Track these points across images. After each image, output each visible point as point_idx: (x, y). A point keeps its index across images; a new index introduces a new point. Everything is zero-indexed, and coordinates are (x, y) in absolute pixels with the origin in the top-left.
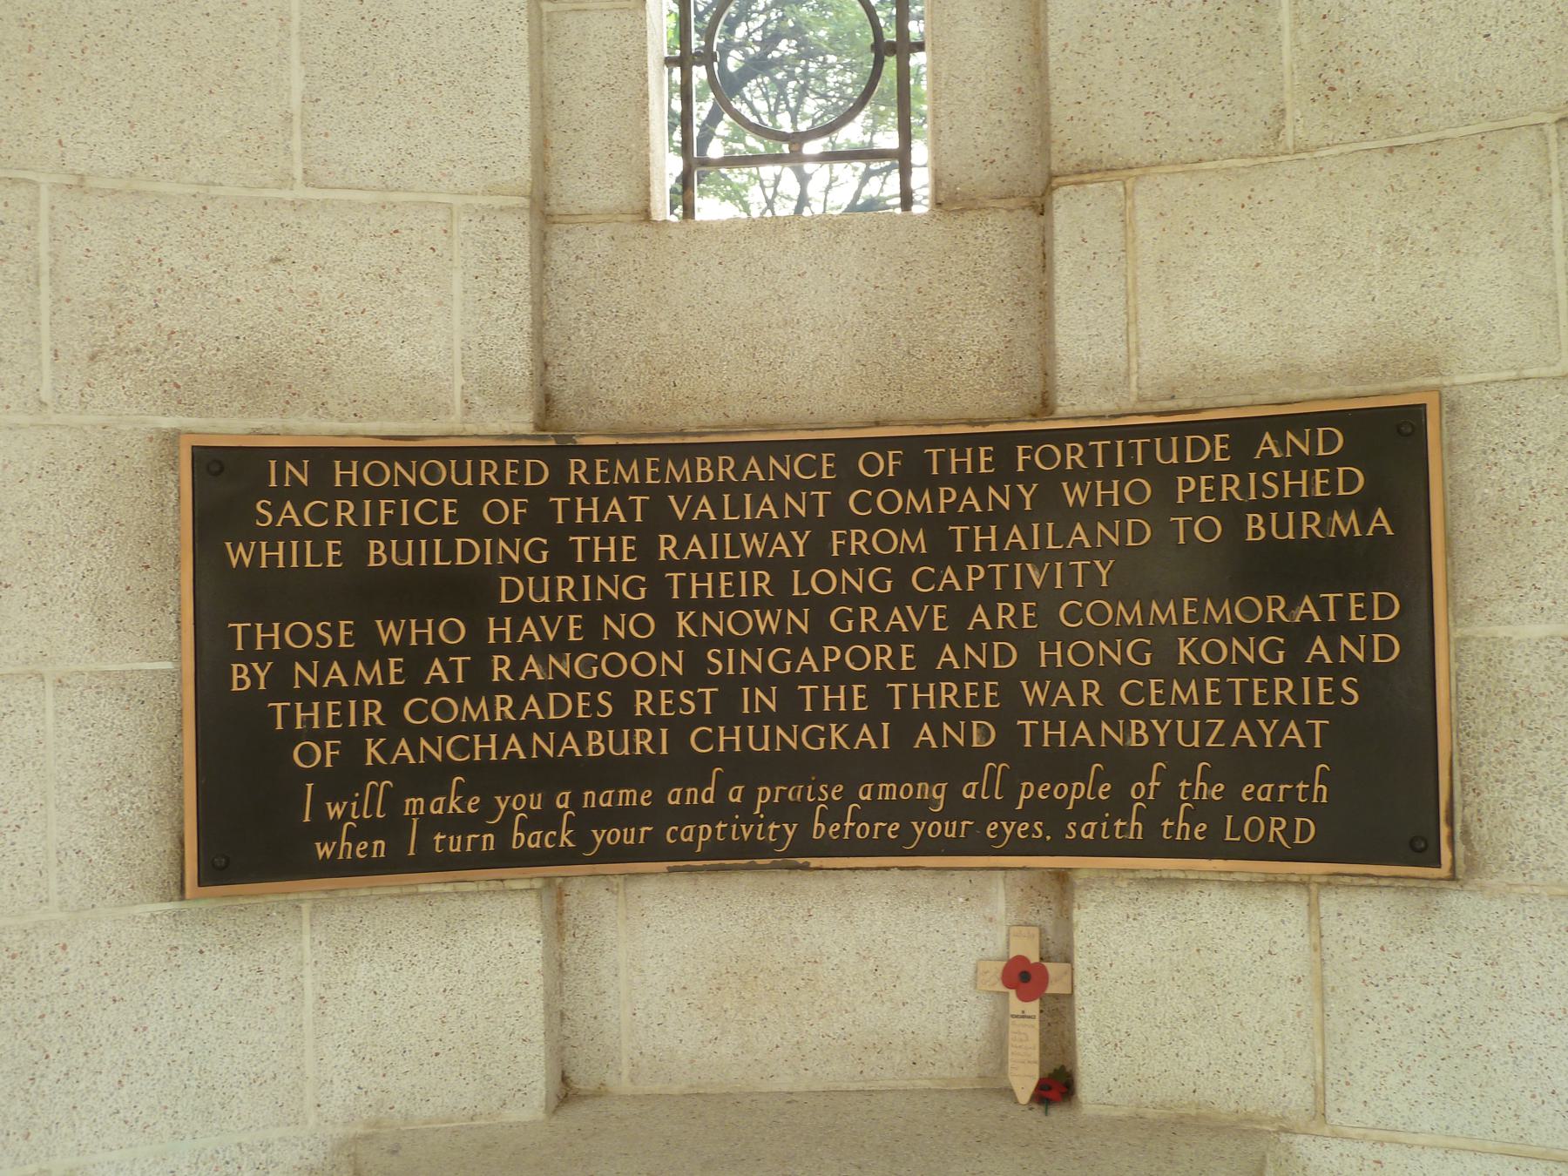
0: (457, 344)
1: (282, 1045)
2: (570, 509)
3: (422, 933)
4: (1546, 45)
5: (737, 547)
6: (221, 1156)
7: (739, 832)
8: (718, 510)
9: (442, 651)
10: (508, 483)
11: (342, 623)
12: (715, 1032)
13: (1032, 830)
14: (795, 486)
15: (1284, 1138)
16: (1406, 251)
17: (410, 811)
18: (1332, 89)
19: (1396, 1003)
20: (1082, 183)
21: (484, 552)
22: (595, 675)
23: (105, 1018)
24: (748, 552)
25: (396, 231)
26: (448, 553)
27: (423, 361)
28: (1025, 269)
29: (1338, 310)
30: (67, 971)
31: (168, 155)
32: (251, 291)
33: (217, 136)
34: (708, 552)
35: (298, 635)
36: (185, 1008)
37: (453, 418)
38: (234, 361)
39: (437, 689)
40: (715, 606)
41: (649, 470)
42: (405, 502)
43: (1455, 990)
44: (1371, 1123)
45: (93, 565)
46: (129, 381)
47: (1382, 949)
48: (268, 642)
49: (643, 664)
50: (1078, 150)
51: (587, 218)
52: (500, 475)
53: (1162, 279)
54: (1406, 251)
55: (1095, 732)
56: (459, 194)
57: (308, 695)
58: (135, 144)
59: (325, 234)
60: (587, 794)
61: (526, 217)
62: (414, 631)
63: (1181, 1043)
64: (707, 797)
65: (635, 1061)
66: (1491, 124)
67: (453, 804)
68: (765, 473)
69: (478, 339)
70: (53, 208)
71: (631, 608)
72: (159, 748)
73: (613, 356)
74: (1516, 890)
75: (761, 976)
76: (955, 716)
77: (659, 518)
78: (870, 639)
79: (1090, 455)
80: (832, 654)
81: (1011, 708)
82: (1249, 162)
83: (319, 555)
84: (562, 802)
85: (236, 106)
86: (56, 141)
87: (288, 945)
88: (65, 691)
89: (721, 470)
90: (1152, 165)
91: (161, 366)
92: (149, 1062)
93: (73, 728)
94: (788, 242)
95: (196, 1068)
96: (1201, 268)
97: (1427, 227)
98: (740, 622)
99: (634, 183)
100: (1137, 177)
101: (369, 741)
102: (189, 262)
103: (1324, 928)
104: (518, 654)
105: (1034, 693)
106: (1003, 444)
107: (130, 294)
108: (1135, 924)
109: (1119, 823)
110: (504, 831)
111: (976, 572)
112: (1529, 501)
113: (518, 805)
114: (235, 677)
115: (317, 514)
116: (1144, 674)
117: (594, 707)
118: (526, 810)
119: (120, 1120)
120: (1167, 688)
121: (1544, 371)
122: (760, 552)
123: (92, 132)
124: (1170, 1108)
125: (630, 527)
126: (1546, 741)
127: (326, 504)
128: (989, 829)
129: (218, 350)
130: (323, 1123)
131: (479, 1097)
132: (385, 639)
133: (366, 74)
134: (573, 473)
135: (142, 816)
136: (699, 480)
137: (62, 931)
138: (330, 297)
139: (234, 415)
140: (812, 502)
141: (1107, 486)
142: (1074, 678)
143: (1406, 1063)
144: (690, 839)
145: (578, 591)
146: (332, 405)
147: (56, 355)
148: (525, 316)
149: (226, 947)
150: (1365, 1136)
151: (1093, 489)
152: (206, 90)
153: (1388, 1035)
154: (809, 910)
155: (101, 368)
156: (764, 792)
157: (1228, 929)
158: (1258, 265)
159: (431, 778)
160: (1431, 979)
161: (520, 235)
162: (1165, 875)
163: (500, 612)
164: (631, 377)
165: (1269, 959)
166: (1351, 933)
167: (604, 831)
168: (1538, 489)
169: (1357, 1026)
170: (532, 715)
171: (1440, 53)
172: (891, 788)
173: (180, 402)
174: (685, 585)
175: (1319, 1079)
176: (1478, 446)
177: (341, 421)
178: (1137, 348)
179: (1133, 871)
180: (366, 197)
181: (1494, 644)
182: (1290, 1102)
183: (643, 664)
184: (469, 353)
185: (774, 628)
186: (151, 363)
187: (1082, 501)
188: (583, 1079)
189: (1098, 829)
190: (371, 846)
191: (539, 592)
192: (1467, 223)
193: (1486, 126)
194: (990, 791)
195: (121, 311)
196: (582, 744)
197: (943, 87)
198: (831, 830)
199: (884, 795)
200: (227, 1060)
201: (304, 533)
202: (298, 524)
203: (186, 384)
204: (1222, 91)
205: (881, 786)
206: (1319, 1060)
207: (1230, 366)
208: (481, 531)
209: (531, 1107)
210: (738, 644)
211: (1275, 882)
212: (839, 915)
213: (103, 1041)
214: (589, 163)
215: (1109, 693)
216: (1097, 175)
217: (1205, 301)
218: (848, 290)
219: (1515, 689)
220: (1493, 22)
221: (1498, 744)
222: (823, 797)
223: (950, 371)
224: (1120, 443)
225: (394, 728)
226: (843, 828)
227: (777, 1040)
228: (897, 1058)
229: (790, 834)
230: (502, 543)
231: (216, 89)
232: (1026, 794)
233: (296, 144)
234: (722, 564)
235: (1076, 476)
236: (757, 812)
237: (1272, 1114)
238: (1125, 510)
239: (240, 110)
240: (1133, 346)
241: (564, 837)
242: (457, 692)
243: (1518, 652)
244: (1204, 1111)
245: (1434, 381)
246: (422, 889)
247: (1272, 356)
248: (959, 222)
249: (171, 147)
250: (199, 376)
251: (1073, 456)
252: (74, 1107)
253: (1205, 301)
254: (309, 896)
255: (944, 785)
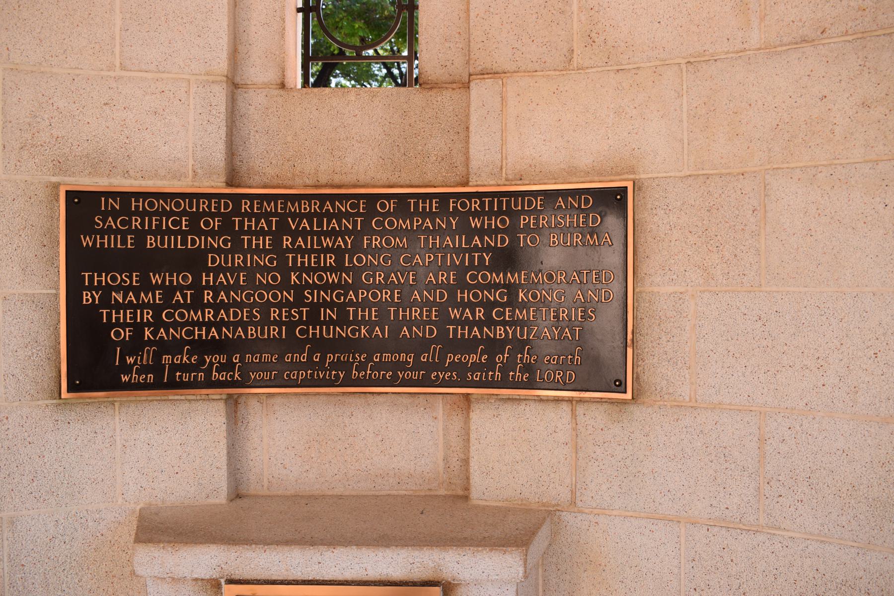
0: (190, 145)
1: (106, 466)
2: (241, 223)
3: (171, 418)
4: (683, 28)
5: (320, 243)
6: (78, 515)
7: (318, 375)
8: (311, 226)
9: (181, 288)
10: (213, 210)
11: (134, 274)
12: (307, 467)
13: (452, 376)
14: (347, 215)
15: (558, 513)
16: (623, 117)
17: (165, 361)
18: (594, 42)
19: (606, 453)
20: (484, 78)
21: (200, 242)
22: (252, 301)
23: (25, 451)
24: (325, 245)
25: (163, 92)
26: (184, 242)
27: (175, 152)
28: (459, 117)
29: (594, 143)
30: (8, 429)
31: (57, 55)
32: (94, 119)
33: (80, 46)
34: (306, 244)
35: (114, 279)
36: (62, 448)
37: (188, 180)
38: (86, 151)
39: (178, 305)
40: (309, 270)
41: (279, 206)
42: (164, 218)
43: (631, 447)
44: (594, 506)
45: (20, 245)
46: (37, 160)
47: (602, 430)
48: (100, 282)
49: (275, 296)
50: (482, 63)
51: (255, 86)
52: (209, 207)
53: (518, 124)
54: (623, 117)
55: (481, 332)
56: (193, 74)
57: (118, 306)
58: (42, 50)
59: (129, 92)
60: (247, 356)
61: (225, 85)
62: (168, 278)
63: (516, 472)
64: (304, 359)
65: (270, 480)
66: (659, 62)
67: (185, 359)
68: (334, 209)
69: (201, 143)
70: (4, 79)
71: (269, 270)
72: (50, 329)
73: (265, 152)
74: (657, 403)
75: (329, 442)
76: (420, 324)
77: (282, 227)
78: (380, 287)
79: (482, 204)
80: (363, 293)
81: (444, 319)
82: (557, 73)
83: (124, 242)
84: (236, 359)
85: (89, 32)
86: (6, 48)
87: (109, 421)
88: (6, 302)
89: (313, 207)
90: (515, 72)
91: (52, 153)
92: (45, 471)
93: (10, 319)
94: (349, 100)
95: (67, 475)
96: (535, 120)
97: (632, 107)
98: (320, 278)
99: (277, 70)
100: (508, 77)
101: (146, 329)
102: (66, 104)
103: (578, 420)
104: (216, 291)
105: (455, 313)
106: (444, 198)
107: (38, 120)
108: (497, 419)
109: (490, 373)
110: (208, 372)
111: (429, 257)
112: (669, 232)
113: (215, 360)
114: (85, 297)
115: (123, 223)
116: (503, 305)
117: (251, 315)
118: (219, 362)
119: (33, 496)
120: (513, 311)
121: (678, 174)
122: (330, 245)
123: (23, 44)
124: (510, 501)
125: (270, 232)
126: (672, 338)
127: (127, 219)
128: (433, 375)
129: (79, 146)
130: (125, 502)
131: (197, 493)
132: (154, 282)
133: (150, 18)
134: (243, 206)
135: (42, 360)
136: (303, 211)
137: (6, 411)
138: (131, 122)
139: (86, 176)
140: (355, 223)
141: (490, 219)
142: (472, 306)
143: (610, 479)
144: (295, 377)
145: (245, 261)
146: (131, 173)
147: (4, 147)
148: (223, 132)
149: (80, 421)
150: (592, 512)
151: (484, 220)
152: (75, 25)
153: (603, 467)
154: (352, 413)
155: (25, 154)
156: (330, 357)
157: (537, 421)
158: (560, 120)
159: (175, 347)
160: (622, 443)
161: (222, 94)
162: (511, 397)
163: (208, 271)
164: (274, 162)
165: (554, 434)
166: (589, 423)
167: (255, 373)
168: (673, 226)
169: (590, 464)
170: (222, 319)
171: (640, 29)
172: (388, 356)
173: (61, 170)
174: (295, 259)
175: (574, 487)
176: (649, 206)
177: (135, 180)
178: (506, 157)
179: (497, 395)
180: (149, 76)
181: (653, 295)
182: (561, 497)
183: (275, 296)
184: (196, 149)
185: (336, 281)
186: (48, 151)
187: (479, 226)
188: (243, 490)
189: (481, 376)
190: (147, 377)
191: (226, 262)
192: (648, 106)
193: (658, 63)
194: (433, 358)
195: (34, 127)
196: (246, 333)
197: (424, 30)
198: (361, 375)
199: (385, 359)
200: (81, 472)
201: (117, 232)
202: (114, 227)
203: (64, 161)
204: (547, 40)
205: (384, 355)
206: (574, 479)
207: (546, 166)
208: (199, 233)
209: (221, 498)
210: (319, 288)
211: (558, 400)
212: (366, 415)
213: (25, 461)
214: (256, 60)
215: (488, 314)
216: (490, 76)
217: (537, 136)
218: (377, 124)
219: (660, 315)
220: (662, 17)
221: (652, 339)
222: (357, 359)
223: (423, 163)
224: (496, 199)
225: (157, 323)
226: (366, 373)
227: (336, 472)
228: (391, 480)
229: (342, 376)
230: (209, 239)
231: (80, 24)
232: (450, 360)
233: (117, 50)
234: (312, 251)
235: (476, 214)
236: (327, 366)
237: (553, 503)
238: (497, 231)
239: (91, 34)
240: (504, 155)
241: (236, 375)
242: (188, 307)
243: (662, 299)
244: (524, 502)
245: (632, 176)
246: (170, 398)
247: (565, 162)
248: (430, 94)
249: (59, 51)
250: (69, 158)
251: (475, 205)
252: (12, 490)
253: (537, 136)
254: (119, 399)
255: (413, 355)
